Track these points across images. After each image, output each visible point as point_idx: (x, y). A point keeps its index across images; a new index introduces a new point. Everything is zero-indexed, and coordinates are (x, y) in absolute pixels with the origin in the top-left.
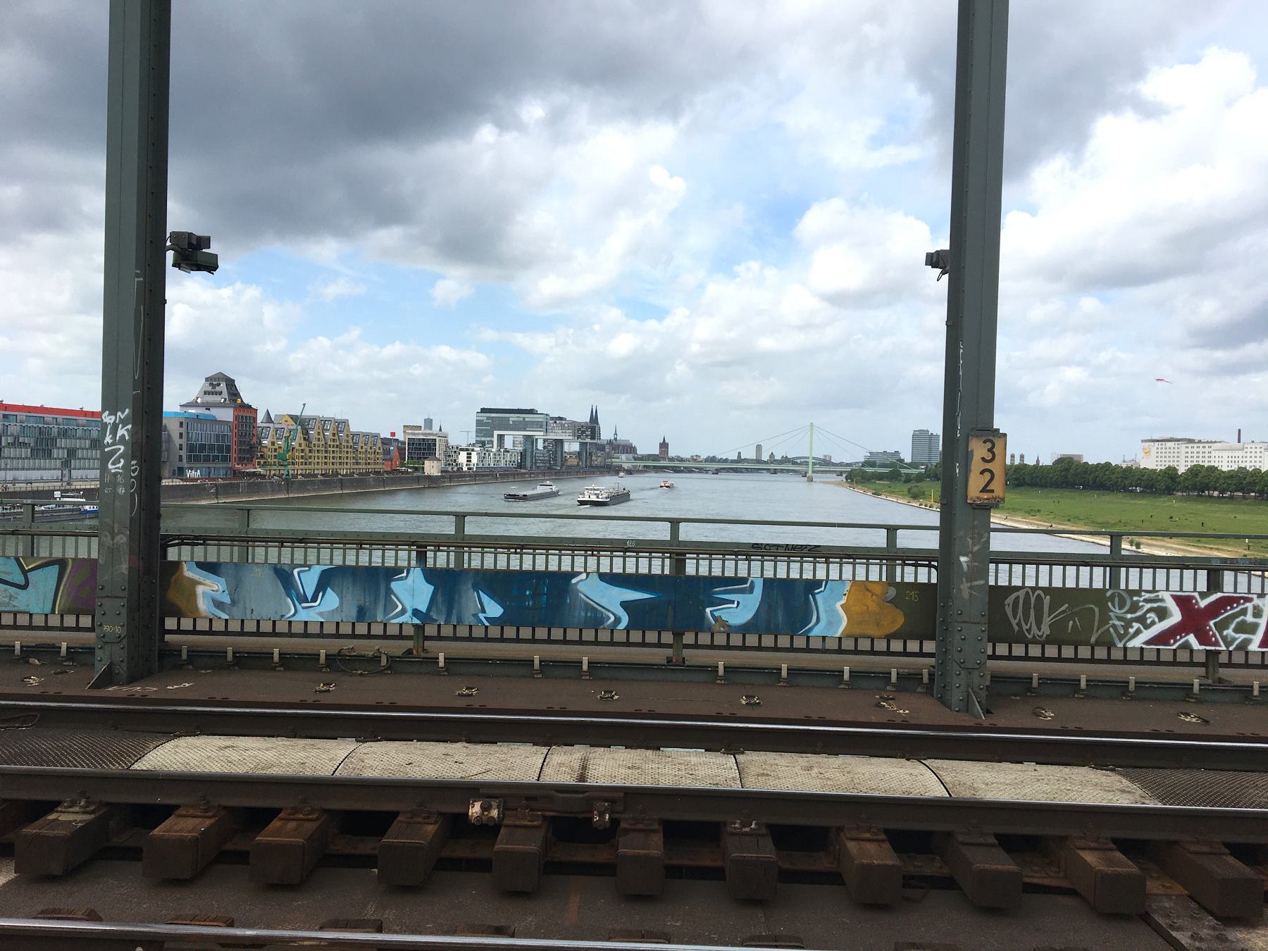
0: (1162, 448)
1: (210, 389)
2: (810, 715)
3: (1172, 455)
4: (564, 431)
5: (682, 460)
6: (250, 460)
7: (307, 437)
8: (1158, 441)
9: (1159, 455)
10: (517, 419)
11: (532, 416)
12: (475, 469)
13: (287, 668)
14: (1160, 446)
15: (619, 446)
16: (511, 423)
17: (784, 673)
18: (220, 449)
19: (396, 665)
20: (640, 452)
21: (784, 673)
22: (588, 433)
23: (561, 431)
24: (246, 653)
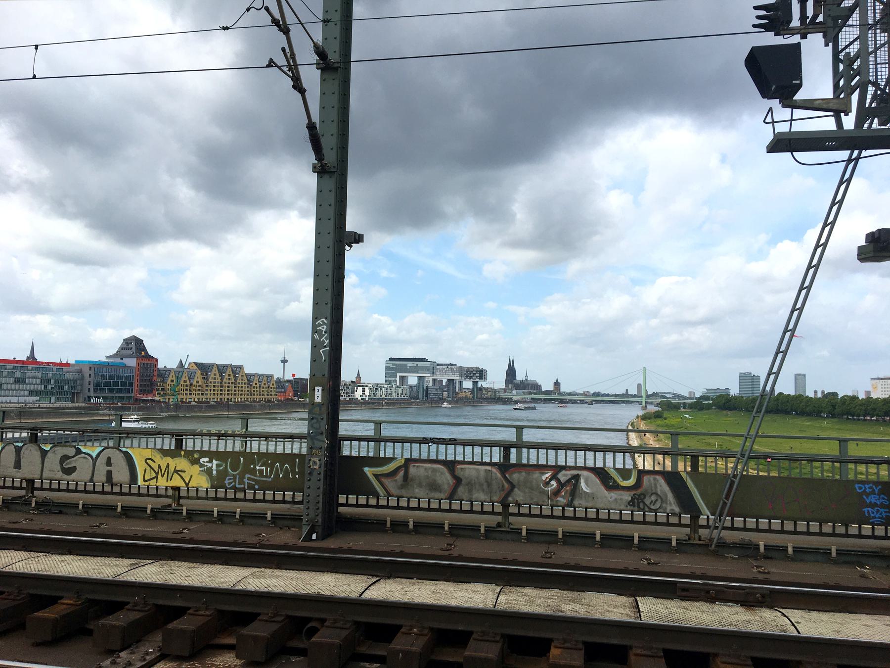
0: (885, 385)
1: (125, 346)
2: (461, 554)
3: (886, 389)
4: (453, 373)
5: (576, 394)
6: (150, 392)
7: (206, 377)
8: (882, 379)
9: (883, 386)
10: (412, 365)
11: (424, 363)
12: (367, 399)
13: (127, 517)
14: (883, 383)
15: (528, 384)
16: (408, 367)
17: (598, 538)
18: (124, 384)
19: (157, 514)
20: (544, 389)
21: (598, 538)
22: (478, 375)
23: (451, 374)
24: (90, 505)
